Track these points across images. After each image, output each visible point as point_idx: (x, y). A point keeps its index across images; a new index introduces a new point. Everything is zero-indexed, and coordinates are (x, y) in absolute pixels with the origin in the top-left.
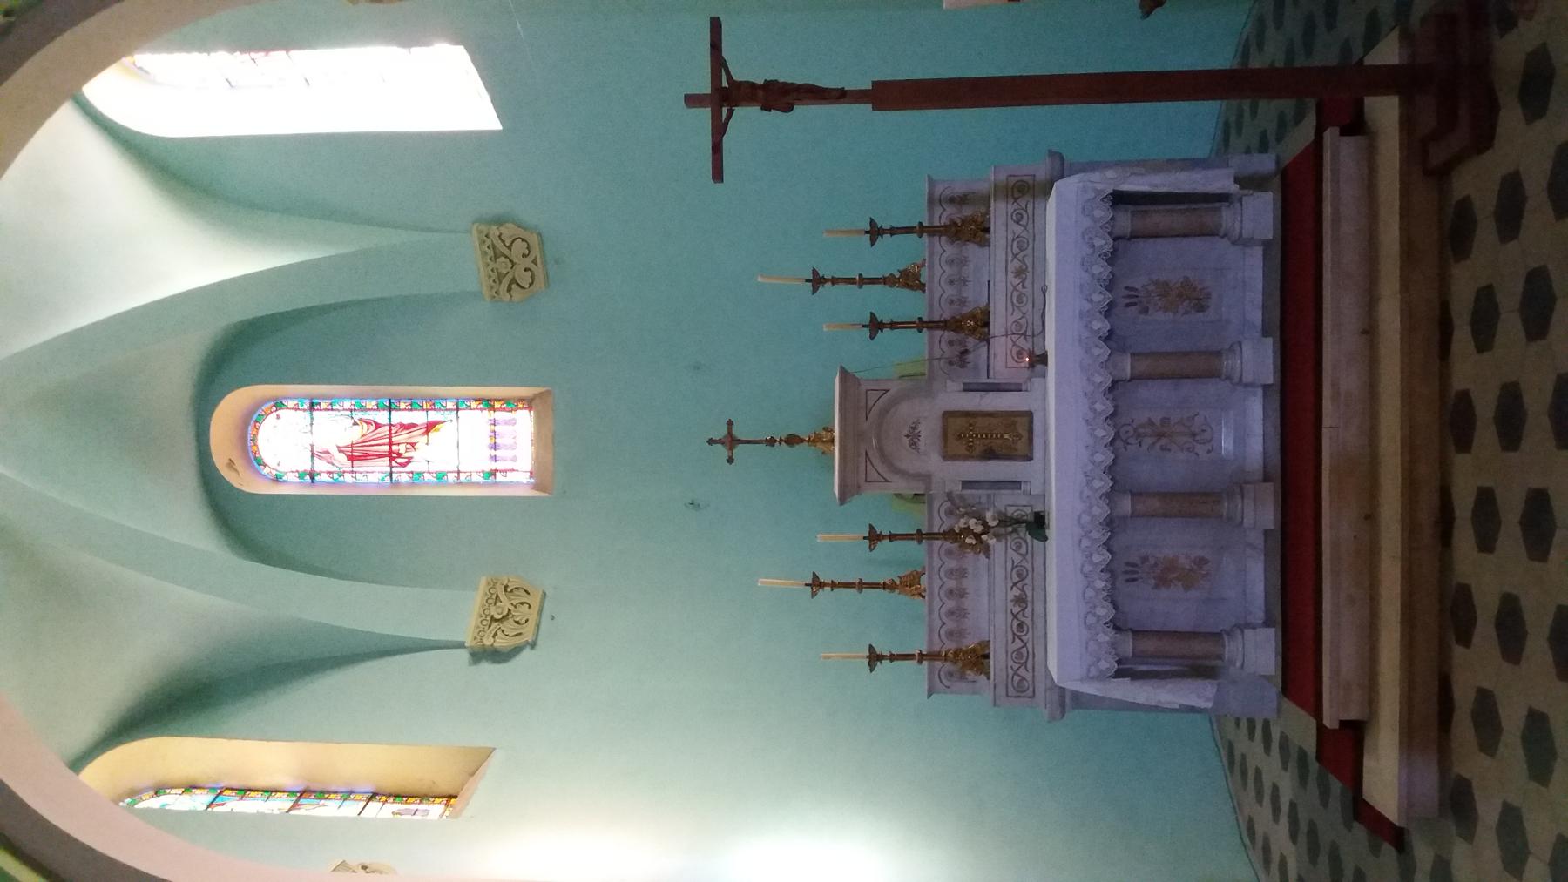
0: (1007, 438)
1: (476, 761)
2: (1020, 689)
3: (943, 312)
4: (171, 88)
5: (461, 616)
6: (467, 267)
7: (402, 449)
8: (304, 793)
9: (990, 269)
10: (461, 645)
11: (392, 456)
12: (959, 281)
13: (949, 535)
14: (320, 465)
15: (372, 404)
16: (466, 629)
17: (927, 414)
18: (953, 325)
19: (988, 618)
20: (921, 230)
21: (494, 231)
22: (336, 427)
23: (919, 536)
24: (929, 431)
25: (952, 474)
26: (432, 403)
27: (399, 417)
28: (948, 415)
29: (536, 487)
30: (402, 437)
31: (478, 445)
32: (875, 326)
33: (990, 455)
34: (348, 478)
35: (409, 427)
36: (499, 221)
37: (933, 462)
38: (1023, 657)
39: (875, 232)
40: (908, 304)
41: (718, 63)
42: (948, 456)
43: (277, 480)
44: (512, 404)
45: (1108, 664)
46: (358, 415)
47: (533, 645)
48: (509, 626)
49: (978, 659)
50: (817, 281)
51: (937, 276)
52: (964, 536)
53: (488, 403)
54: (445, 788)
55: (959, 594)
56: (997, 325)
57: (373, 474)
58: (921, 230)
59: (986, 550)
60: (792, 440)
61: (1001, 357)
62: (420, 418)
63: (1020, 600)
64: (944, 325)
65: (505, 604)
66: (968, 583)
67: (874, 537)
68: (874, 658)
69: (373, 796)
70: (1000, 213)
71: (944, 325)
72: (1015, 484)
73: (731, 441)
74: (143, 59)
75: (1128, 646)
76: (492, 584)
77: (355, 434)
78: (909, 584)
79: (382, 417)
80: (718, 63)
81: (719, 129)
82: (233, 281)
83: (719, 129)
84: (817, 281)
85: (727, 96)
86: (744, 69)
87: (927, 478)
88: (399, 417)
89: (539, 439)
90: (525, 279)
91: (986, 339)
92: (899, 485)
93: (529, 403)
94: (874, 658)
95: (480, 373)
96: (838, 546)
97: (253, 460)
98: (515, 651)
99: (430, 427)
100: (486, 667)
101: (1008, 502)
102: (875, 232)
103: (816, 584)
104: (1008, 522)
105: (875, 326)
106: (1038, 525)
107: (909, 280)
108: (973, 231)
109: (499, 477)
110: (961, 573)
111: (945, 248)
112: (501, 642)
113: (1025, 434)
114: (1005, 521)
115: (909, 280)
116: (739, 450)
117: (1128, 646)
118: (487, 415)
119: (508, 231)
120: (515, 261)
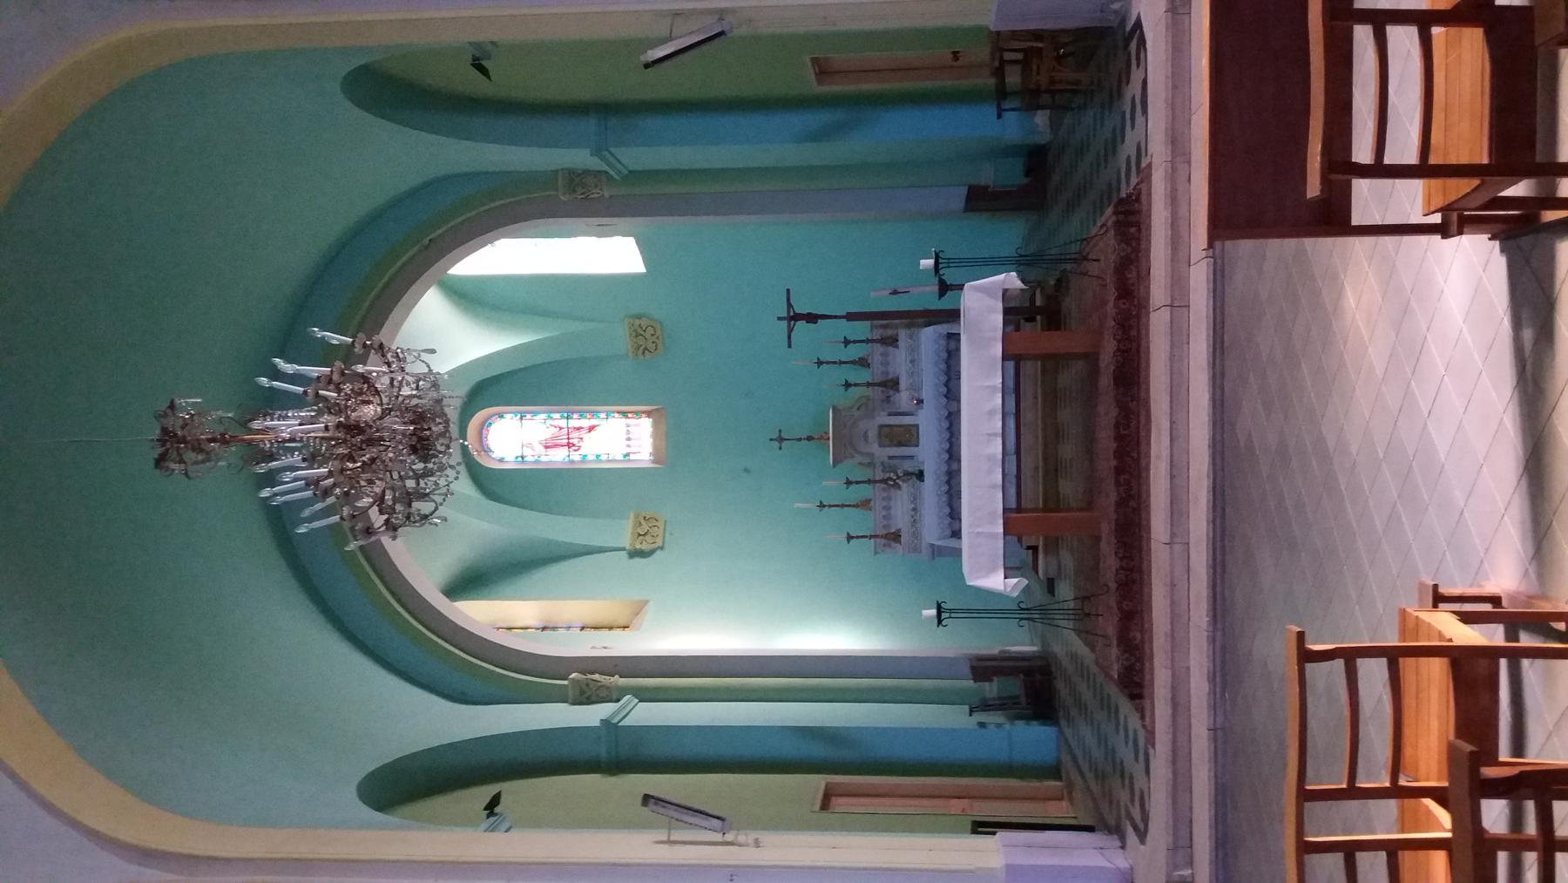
0: (905, 436)
1: (639, 608)
2: (916, 549)
3: (878, 379)
5: (623, 534)
6: (620, 339)
7: (575, 441)
8: (544, 629)
9: (899, 362)
10: (623, 549)
11: (569, 445)
12: (886, 364)
13: (881, 481)
14: (527, 452)
15: (557, 416)
16: (626, 541)
17: (871, 427)
18: (883, 384)
19: (901, 521)
20: (868, 341)
21: (637, 322)
23: (869, 482)
24: (873, 434)
25: (882, 453)
26: (593, 414)
27: (574, 423)
28: (881, 427)
29: (654, 462)
30: (575, 435)
31: (620, 438)
32: (847, 385)
33: (900, 444)
34: (544, 459)
35: (579, 429)
36: (639, 317)
37: (875, 448)
38: (916, 535)
40: (862, 376)
41: (790, 305)
42: (917, 426)
43: (501, 460)
44: (638, 414)
45: (948, 532)
46: (549, 422)
47: (662, 548)
48: (648, 538)
49: (895, 537)
50: (820, 363)
51: (876, 360)
52: (890, 483)
53: (625, 414)
54: (623, 623)
55: (888, 508)
56: (903, 384)
57: (559, 456)
58: (868, 341)
59: (899, 487)
60: (809, 438)
61: (904, 398)
62: (585, 423)
63: (914, 509)
64: (879, 385)
65: (645, 527)
66: (892, 503)
67: (849, 483)
68: (850, 538)
69: (583, 628)
70: (903, 334)
71: (879, 385)
72: (912, 457)
73: (781, 440)
76: (637, 516)
78: (865, 504)
79: (563, 423)
80: (790, 305)
81: (790, 330)
82: (498, 353)
83: (790, 330)
84: (820, 363)
85: (794, 318)
86: (800, 308)
87: (871, 455)
88: (574, 423)
89: (656, 435)
90: (651, 346)
91: (898, 390)
92: (859, 458)
93: (649, 414)
94: (850, 538)
95: (621, 398)
96: (832, 487)
97: (486, 450)
98: (652, 552)
99: (591, 429)
100: (637, 560)
101: (908, 466)
102: (847, 342)
103: (822, 506)
105: (847, 385)
106: (920, 475)
107: (863, 362)
108: (892, 341)
109: (632, 457)
110: (889, 499)
111: (879, 348)
112: (645, 547)
114: (907, 474)
115: (863, 362)
116: (785, 444)
118: (624, 421)
119: (644, 322)
120: (647, 338)
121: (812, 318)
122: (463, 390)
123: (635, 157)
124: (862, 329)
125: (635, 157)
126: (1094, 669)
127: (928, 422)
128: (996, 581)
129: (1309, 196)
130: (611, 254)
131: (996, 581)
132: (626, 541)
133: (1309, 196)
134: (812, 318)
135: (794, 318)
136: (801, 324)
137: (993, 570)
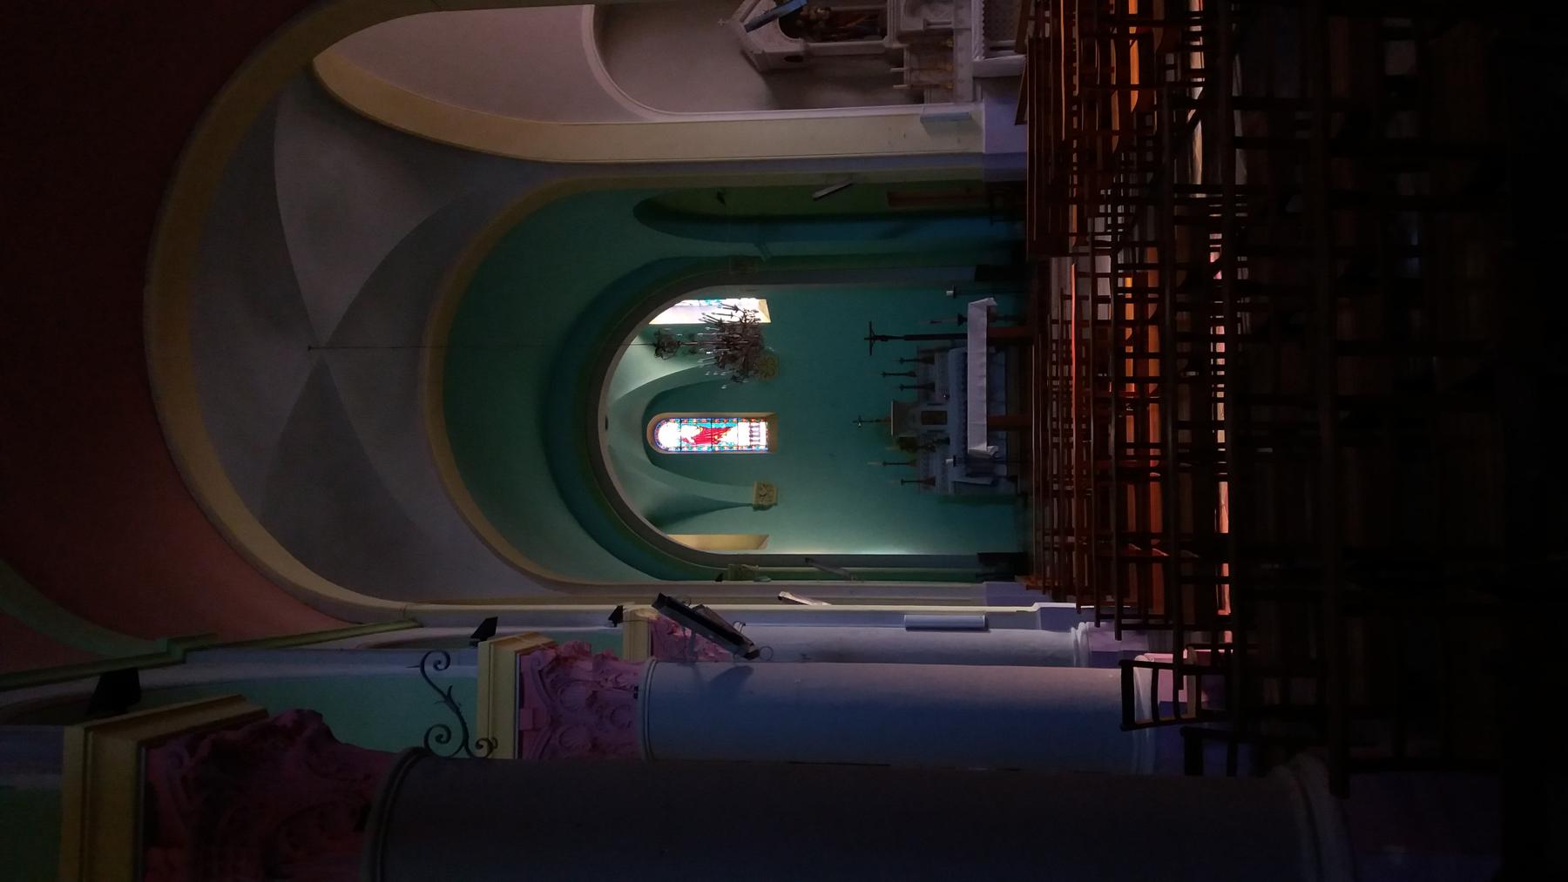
4: (684, 313)
9: (934, 372)
16: (752, 499)
22: (691, 430)
26: (727, 418)
31: (745, 436)
32: (902, 387)
39: (902, 361)
40: (912, 381)
44: (758, 419)
53: (749, 419)
61: (938, 396)
62: (723, 426)
65: (764, 491)
70: (937, 356)
74: (687, 303)
75: (949, 43)
77: (698, 432)
85: (873, 338)
95: (745, 409)
97: (657, 442)
99: (727, 429)
100: (759, 512)
101: (940, 436)
102: (902, 361)
104: (940, 442)
105: (902, 387)
106: (947, 441)
107: (912, 374)
108: (930, 361)
112: (765, 503)
113: (953, 389)
115: (912, 374)
117: (949, 43)
121: (884, 338)
122: (646, 401)
123: (779, 248)
124: (910, 350)
125: (779, 248)
126: (794, 46)
127: (951, 409)
128: (983, 447)
129: (764, 317)
130: (753, 309)
131: (983, 447)
132: (752, 499)
133: (764, 317)
134: (884, 338)
135: (873, 338)
136: (878, 343)
137: (980, 442)
